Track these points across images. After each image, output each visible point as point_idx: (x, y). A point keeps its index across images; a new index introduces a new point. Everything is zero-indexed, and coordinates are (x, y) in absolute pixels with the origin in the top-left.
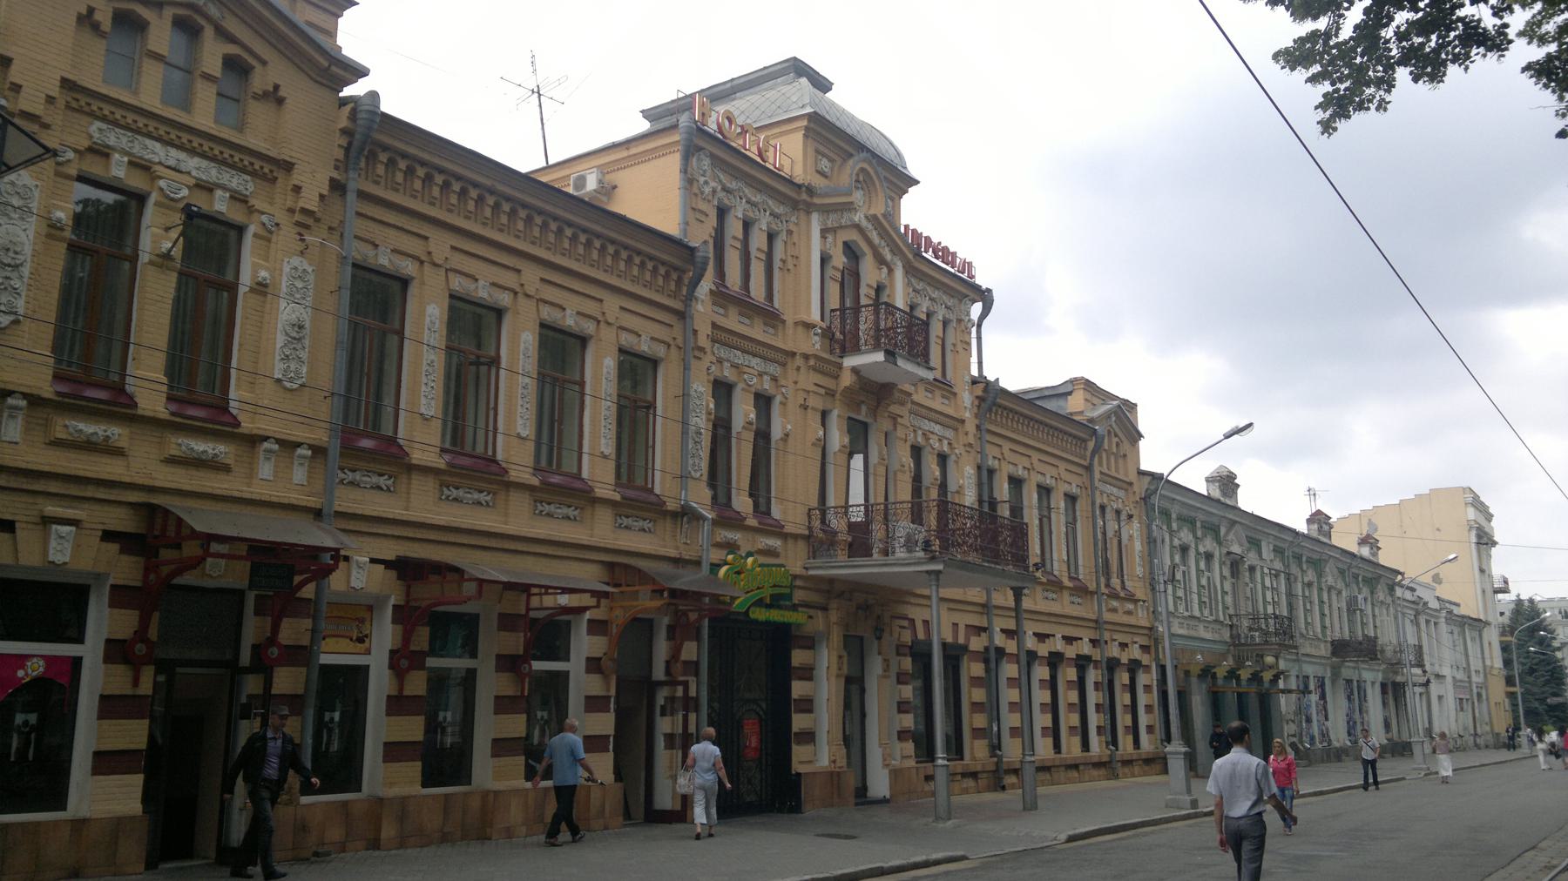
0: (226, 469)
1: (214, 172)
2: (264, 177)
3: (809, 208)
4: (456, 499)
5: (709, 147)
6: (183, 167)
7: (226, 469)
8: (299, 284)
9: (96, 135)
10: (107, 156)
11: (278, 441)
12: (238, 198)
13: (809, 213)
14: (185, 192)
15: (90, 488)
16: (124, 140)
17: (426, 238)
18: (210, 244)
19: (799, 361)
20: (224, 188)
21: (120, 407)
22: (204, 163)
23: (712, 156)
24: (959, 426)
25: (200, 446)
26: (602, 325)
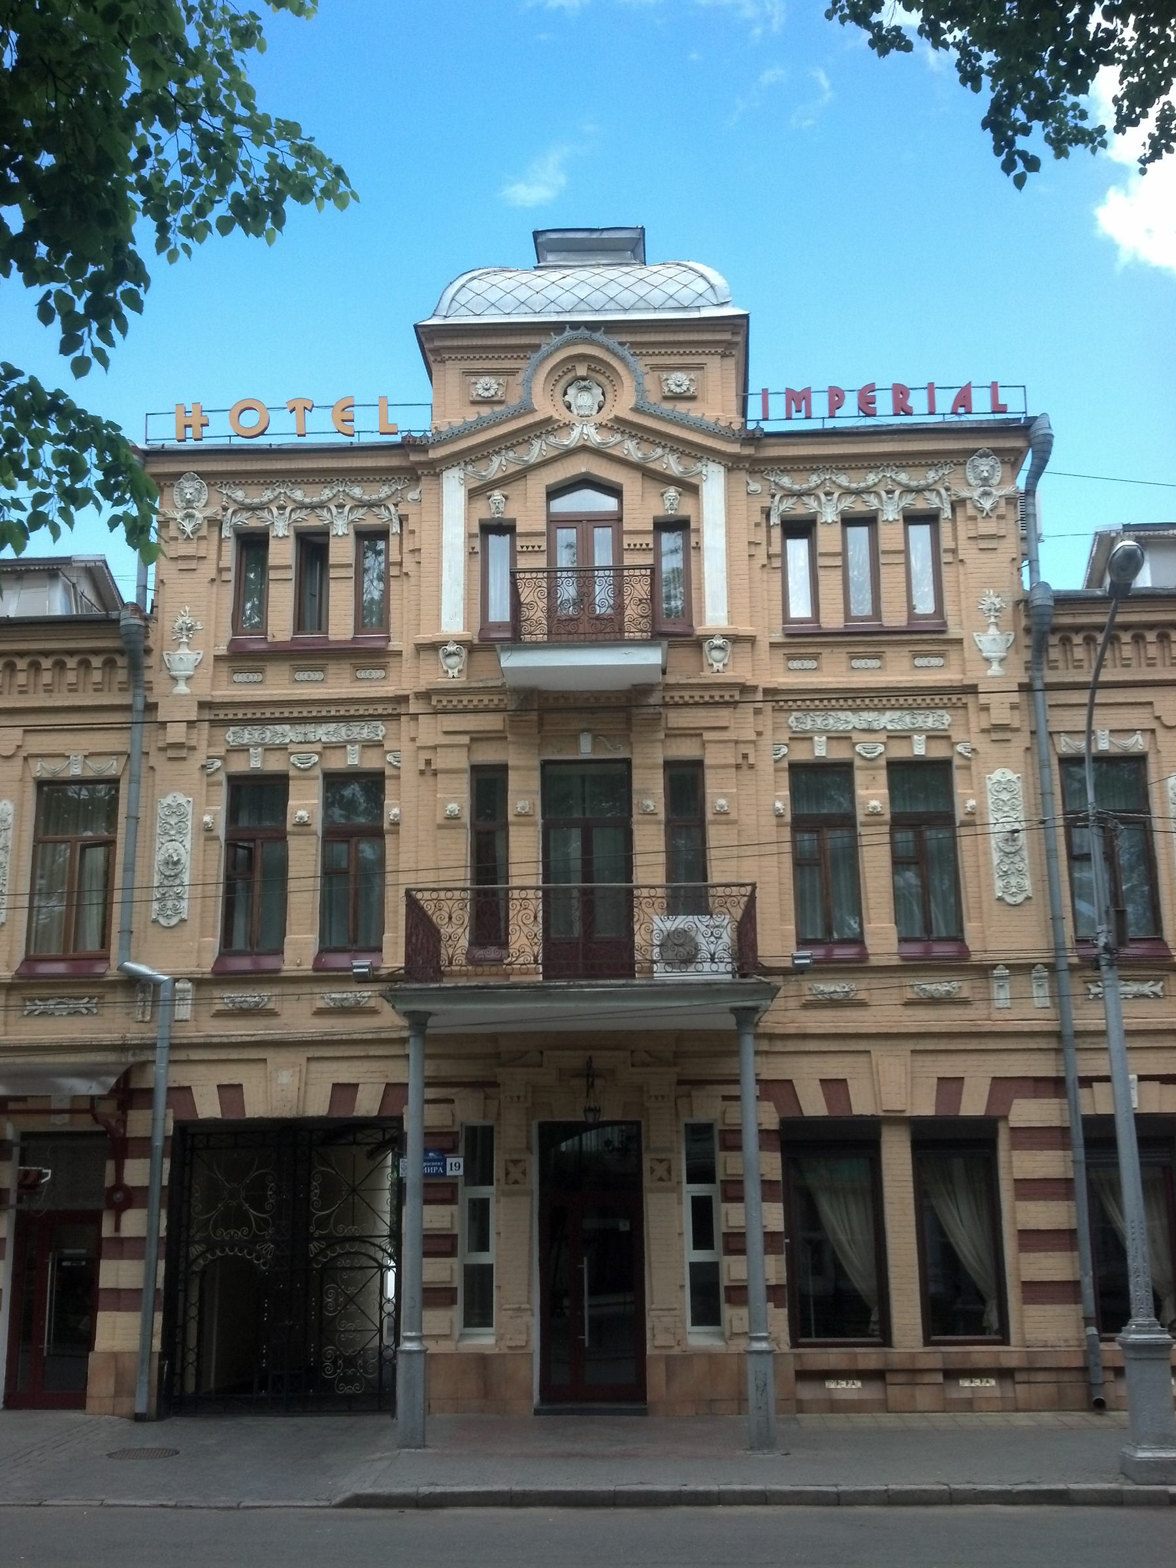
0: (965, 1002)
1: (908, 719)
2: (954, 707)
3: (434, 470)
4: (42, 1014)
5: (985, 444)
6: (875, 726)
7: (965, 1002)
8: (1005, 796)
9: (794, 724)
10: (811, 739)
11: (1007, 966)
12: (933, 737)
13: (438, 475)
14: (881, 749)
15: (1089, 1040)
16: (819, 720)
17: (1151, 703)
18: (924, 786)
19: (413, 707)
20: (919, 730)
21: (860, 966)
22: (332, 727)
23: (202, 475)
24: (968, 699)
25: (939, 986)
26: (1160, 732)
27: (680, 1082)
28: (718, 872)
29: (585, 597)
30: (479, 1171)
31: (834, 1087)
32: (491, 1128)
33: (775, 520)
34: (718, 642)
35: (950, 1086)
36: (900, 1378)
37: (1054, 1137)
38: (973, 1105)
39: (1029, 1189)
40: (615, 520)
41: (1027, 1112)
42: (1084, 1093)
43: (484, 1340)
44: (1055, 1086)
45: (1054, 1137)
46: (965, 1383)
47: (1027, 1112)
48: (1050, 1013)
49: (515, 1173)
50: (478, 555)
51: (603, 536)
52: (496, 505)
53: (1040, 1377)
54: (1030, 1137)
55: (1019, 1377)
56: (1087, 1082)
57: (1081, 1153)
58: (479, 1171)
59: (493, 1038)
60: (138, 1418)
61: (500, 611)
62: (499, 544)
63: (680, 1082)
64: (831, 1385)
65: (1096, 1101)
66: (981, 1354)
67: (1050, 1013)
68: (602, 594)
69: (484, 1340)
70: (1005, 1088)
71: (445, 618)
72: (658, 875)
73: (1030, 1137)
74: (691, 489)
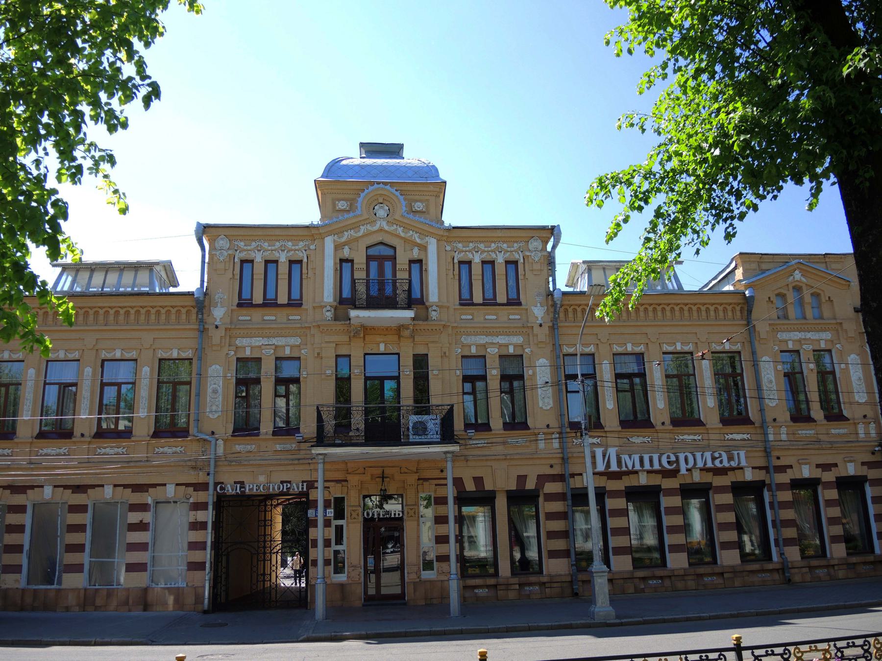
27: (419, 479)
28: (434, 401)
29: (381, 289)
30: (340, 515)
31: (478, 481)
32: (343, 498)
33: (456, 261)
34: (434, 308)
35: (522, 479)
36: (503, 587)
37: (561, 497)
38: (530, 485)
39: (550, 516)
40: (393, 259)
41: (551, 488)
42: (571, 480)
43: (342, 578)
44: (561, 478)
45: (561, 497)
46: (527, 588)
47: (551, 488)
48: (559, 451)
49: (354, 515)
50: (339, 272)
51: (388, 265)
52: (346, 253)
53: (555, 585)
54: (550, 497)
55: (547, 585)
56: (573, 475)
57: (570, 502)
58: (340, 515)
59: (345, 463)
60: (205, 612)
61: (346, 294)
62: (347, 266)
63: (419, 479)
64: (476, 591)
65: (576, 483)
66: (533, 579)
67: (559, 451)
68: (389, 290)
69: (342, 578)
70: (542, 479)
71: (326, 295)
72: (411, 402)
73: (550, 497)
74: (424, 248)
